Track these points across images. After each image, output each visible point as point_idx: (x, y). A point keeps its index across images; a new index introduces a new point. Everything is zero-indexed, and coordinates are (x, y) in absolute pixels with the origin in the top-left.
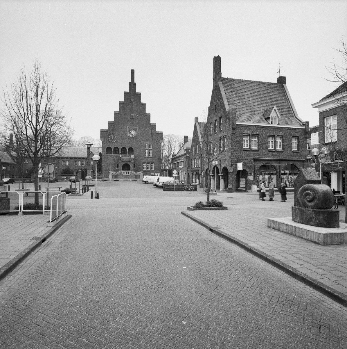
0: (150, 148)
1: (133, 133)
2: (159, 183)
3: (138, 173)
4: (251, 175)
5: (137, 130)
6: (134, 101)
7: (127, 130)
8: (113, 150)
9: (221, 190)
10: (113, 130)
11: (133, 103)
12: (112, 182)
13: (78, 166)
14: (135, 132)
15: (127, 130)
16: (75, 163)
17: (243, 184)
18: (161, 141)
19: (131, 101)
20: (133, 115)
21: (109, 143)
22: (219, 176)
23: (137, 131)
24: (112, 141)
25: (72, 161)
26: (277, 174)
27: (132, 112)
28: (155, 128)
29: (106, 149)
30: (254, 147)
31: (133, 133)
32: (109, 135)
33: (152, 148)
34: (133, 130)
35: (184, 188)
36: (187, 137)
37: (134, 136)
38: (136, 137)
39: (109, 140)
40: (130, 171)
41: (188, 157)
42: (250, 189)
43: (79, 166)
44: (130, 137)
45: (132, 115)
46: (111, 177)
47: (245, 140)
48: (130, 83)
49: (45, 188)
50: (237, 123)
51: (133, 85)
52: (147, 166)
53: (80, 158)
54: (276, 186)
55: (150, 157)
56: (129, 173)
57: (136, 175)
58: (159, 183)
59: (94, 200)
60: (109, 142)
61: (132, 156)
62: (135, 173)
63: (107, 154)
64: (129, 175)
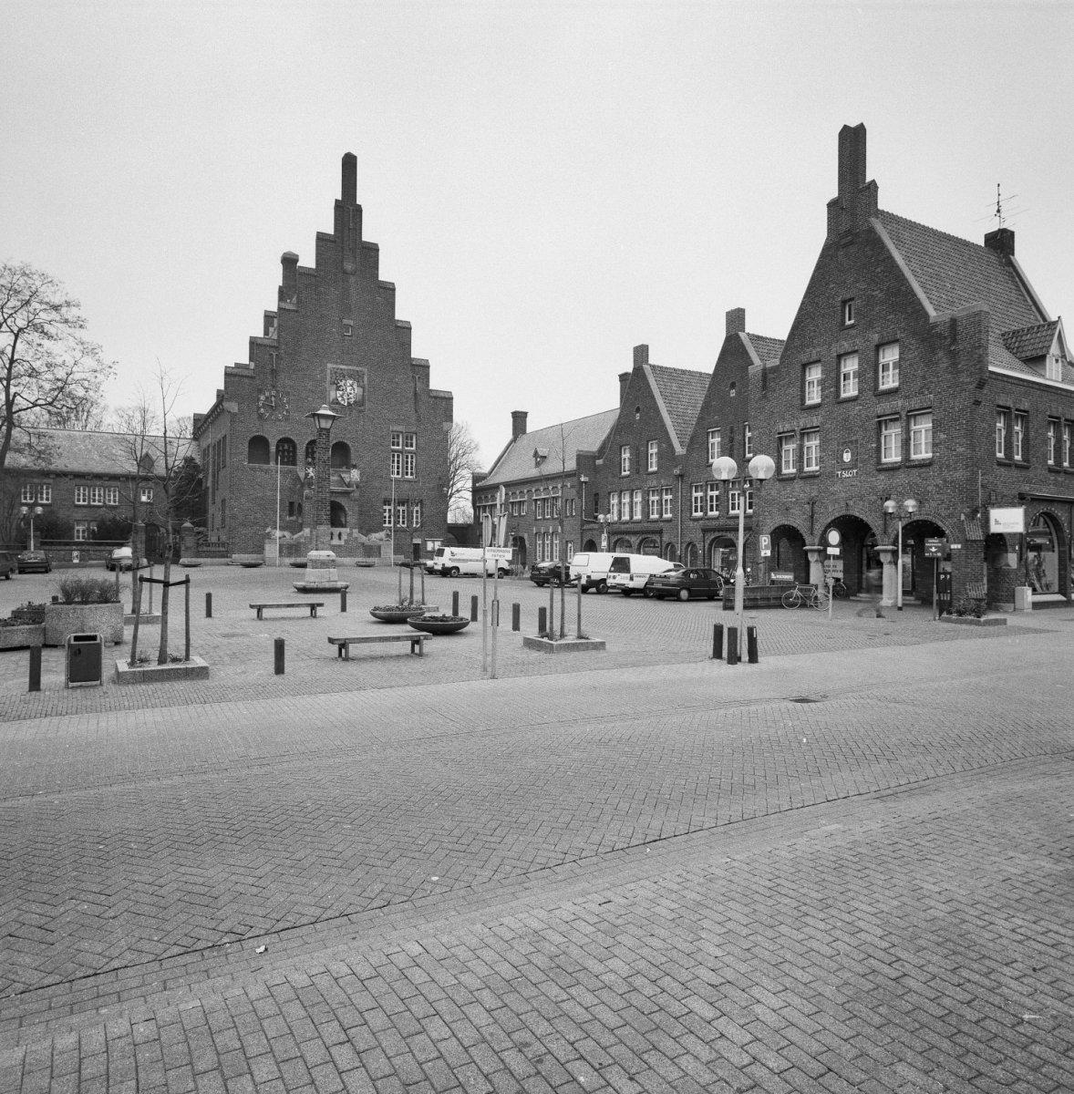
0: (407, 446)
1: (349, 389)
2: (632, 579)
3: (375, 537)
4: (1014, 551)
5: (366, 379)
6: (353, 274)
7: (328, 378)
8: (273, 449)
9: (886, 600)
10: (274, 372)
11: (352, 279)
12: (285, 570)
13: (89, 506)
14: (355, 386)
15: (328, 378)
16: (79, 495)
17: (732, 581)
18: (446, 426)
19: (345, 272)
20: (352, 323)
21: (257, 423)
22: (806, 552)
23: (366, 382)
24: (271, 415)
25: (65, 483)
26: (1061, 549)
27: (346, 310)
28: (427, 376)
29: (246, 445)
30: (923, 453)
31: (348, 391)
32: (260, 391)
33: (414, 448)
34: (351, 377)
35: (787, 598)
36: (525, 414)
37: (352, 401)
38: (360, 403)
39: (259, 408)
40: (345, 531)
41: (586, 483)
42: (1011, 598)
43: (94, 506)
44: (338, 403)
45: (345, 321)
46: (271, 550)
47: (923, 431)
48: (336, 200)
49: (252, 607)
50: (991, 368)
51: (348, 211)
52: (399, 511)
53: (99, 476)
54: (1056, 588)
55: (409, 481)
56: (340, 538)
57: (367, 543)
58: (632, 579)
59: (743, 668)
60: (261, 416)
61: (355, 475)
62: (364, 539)
63: (249, 463)
64: (342, 543)
